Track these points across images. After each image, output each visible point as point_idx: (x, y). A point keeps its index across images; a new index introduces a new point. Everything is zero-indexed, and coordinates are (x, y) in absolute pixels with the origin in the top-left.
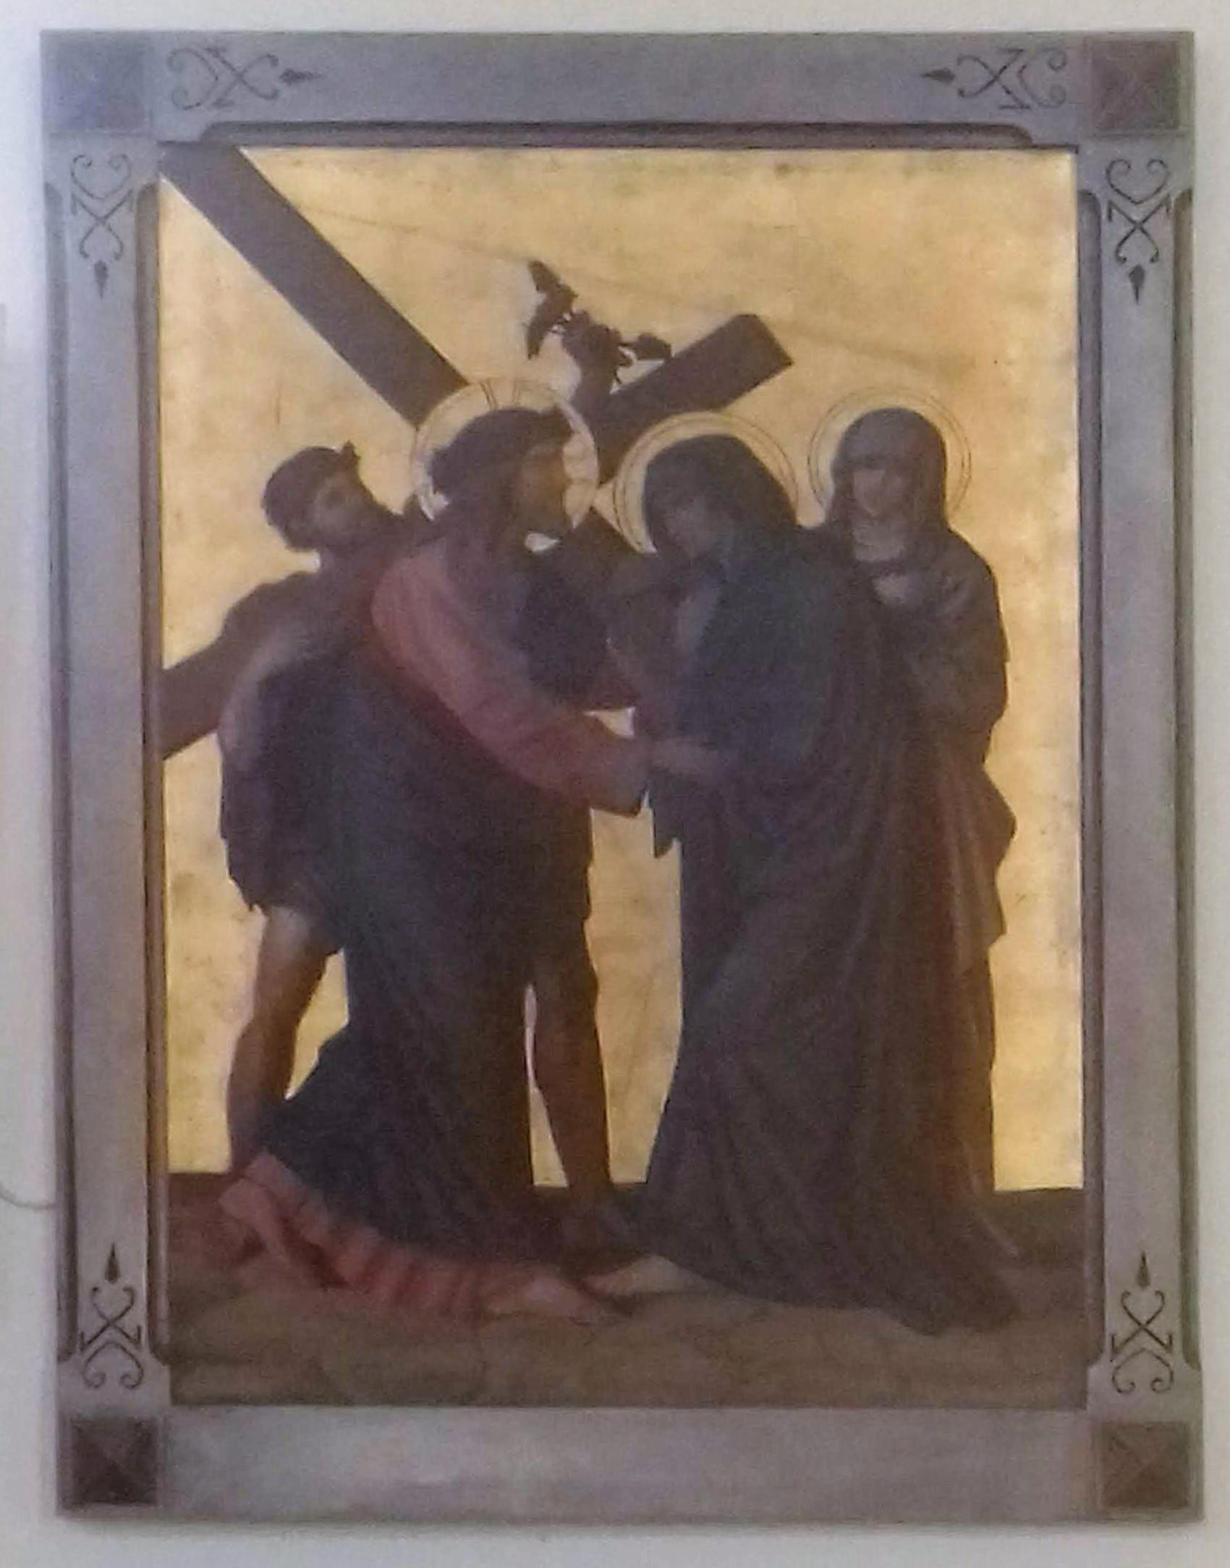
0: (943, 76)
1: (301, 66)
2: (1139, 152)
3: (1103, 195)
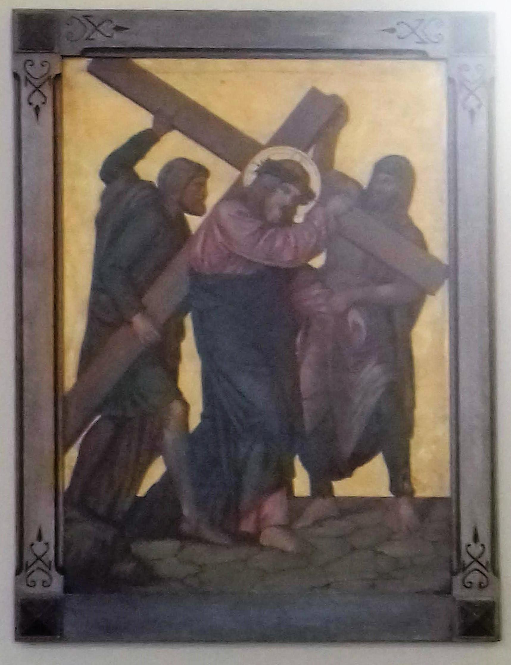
3: (490, 574)
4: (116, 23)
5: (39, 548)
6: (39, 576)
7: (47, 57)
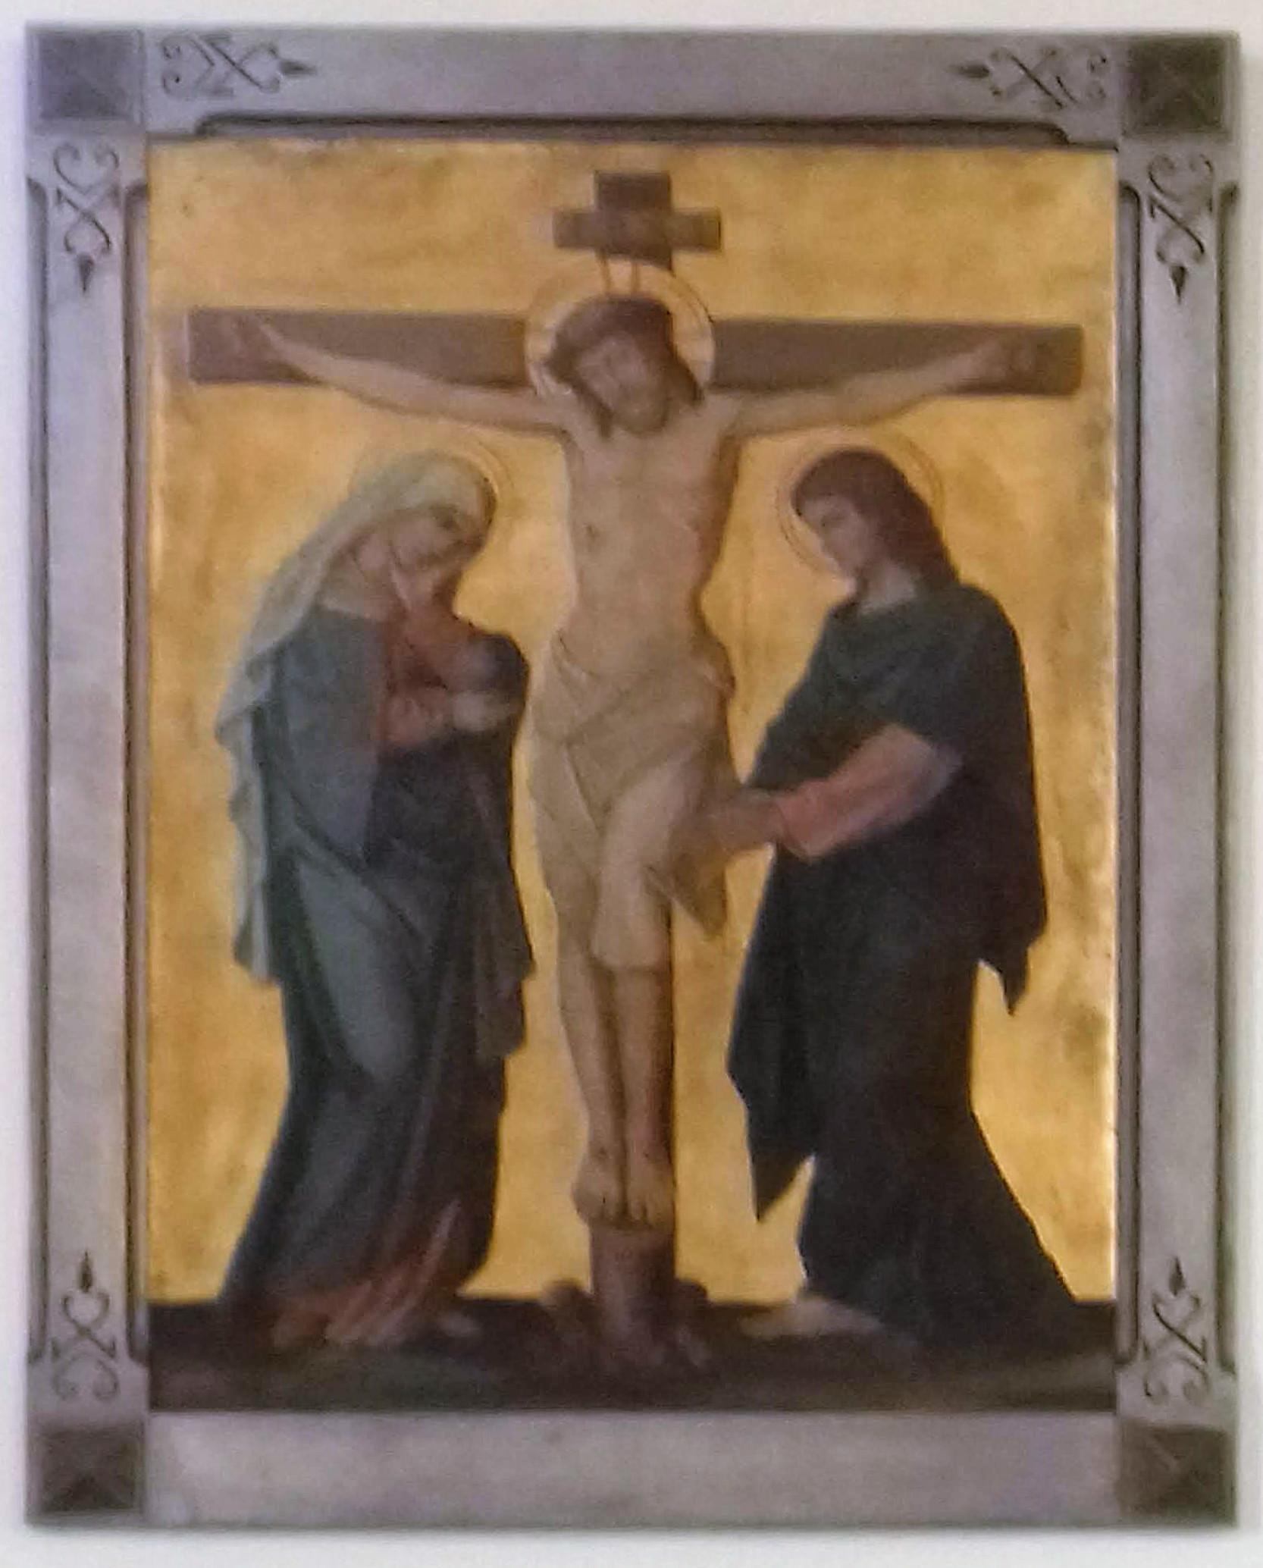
2: (1180, 149)
5: (85, 1308)
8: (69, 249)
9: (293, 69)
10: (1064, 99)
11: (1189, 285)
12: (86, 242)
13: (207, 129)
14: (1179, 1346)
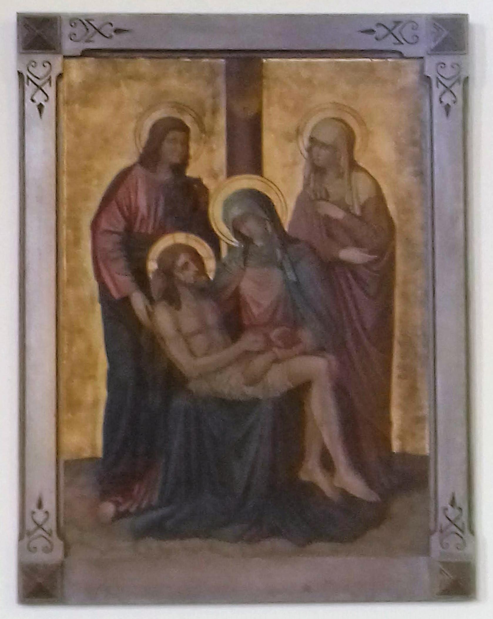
0: (371, 31)
1: (121, 26)
2: (448, 60)
3: (26, 73)
4: (116, 26)
5: (40, 517)
6: (448, 72)
7: (48, 57)
8: (33, 101)
9: (118, 31)
10: (403, 41)
11: (451, 113)
12: (447, 99)
13: (86, 53)
14: (454, 528)
